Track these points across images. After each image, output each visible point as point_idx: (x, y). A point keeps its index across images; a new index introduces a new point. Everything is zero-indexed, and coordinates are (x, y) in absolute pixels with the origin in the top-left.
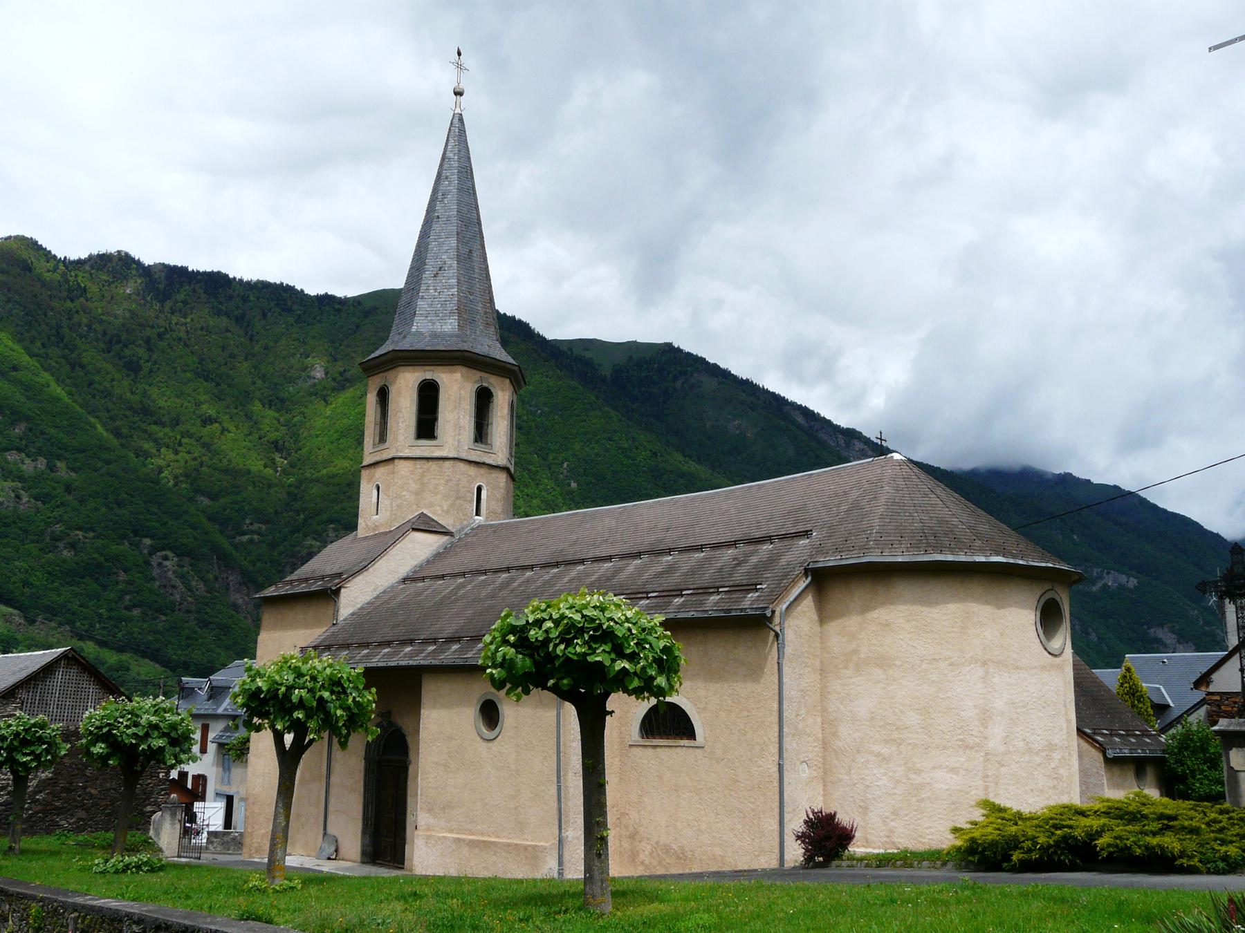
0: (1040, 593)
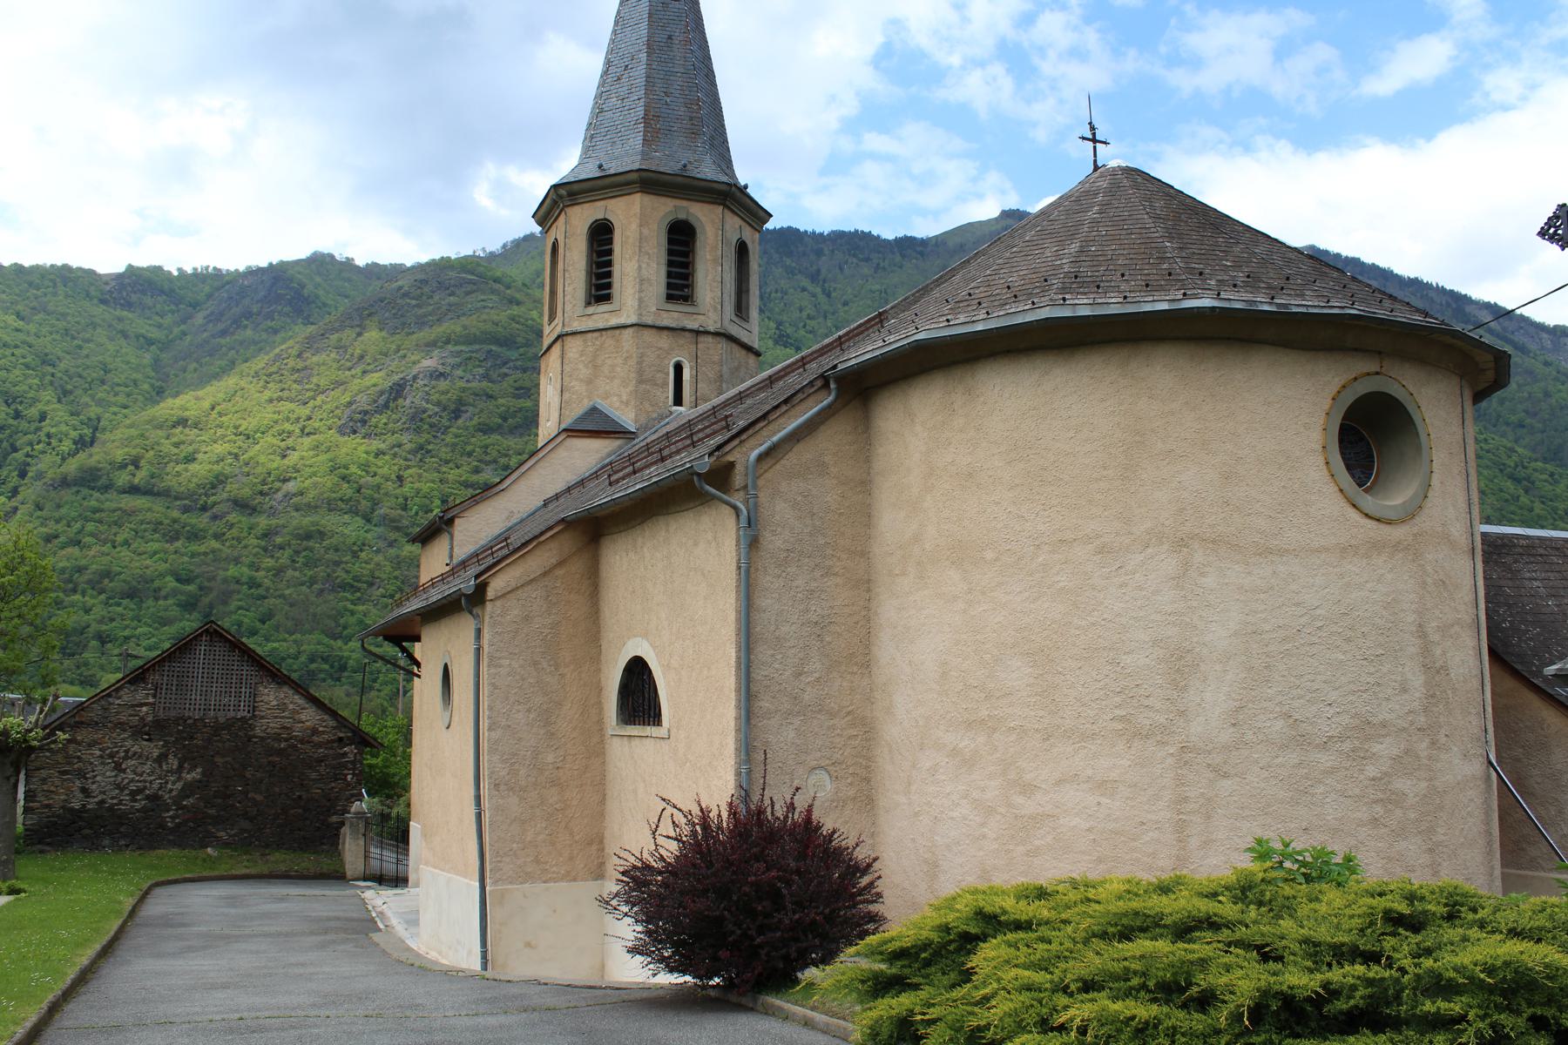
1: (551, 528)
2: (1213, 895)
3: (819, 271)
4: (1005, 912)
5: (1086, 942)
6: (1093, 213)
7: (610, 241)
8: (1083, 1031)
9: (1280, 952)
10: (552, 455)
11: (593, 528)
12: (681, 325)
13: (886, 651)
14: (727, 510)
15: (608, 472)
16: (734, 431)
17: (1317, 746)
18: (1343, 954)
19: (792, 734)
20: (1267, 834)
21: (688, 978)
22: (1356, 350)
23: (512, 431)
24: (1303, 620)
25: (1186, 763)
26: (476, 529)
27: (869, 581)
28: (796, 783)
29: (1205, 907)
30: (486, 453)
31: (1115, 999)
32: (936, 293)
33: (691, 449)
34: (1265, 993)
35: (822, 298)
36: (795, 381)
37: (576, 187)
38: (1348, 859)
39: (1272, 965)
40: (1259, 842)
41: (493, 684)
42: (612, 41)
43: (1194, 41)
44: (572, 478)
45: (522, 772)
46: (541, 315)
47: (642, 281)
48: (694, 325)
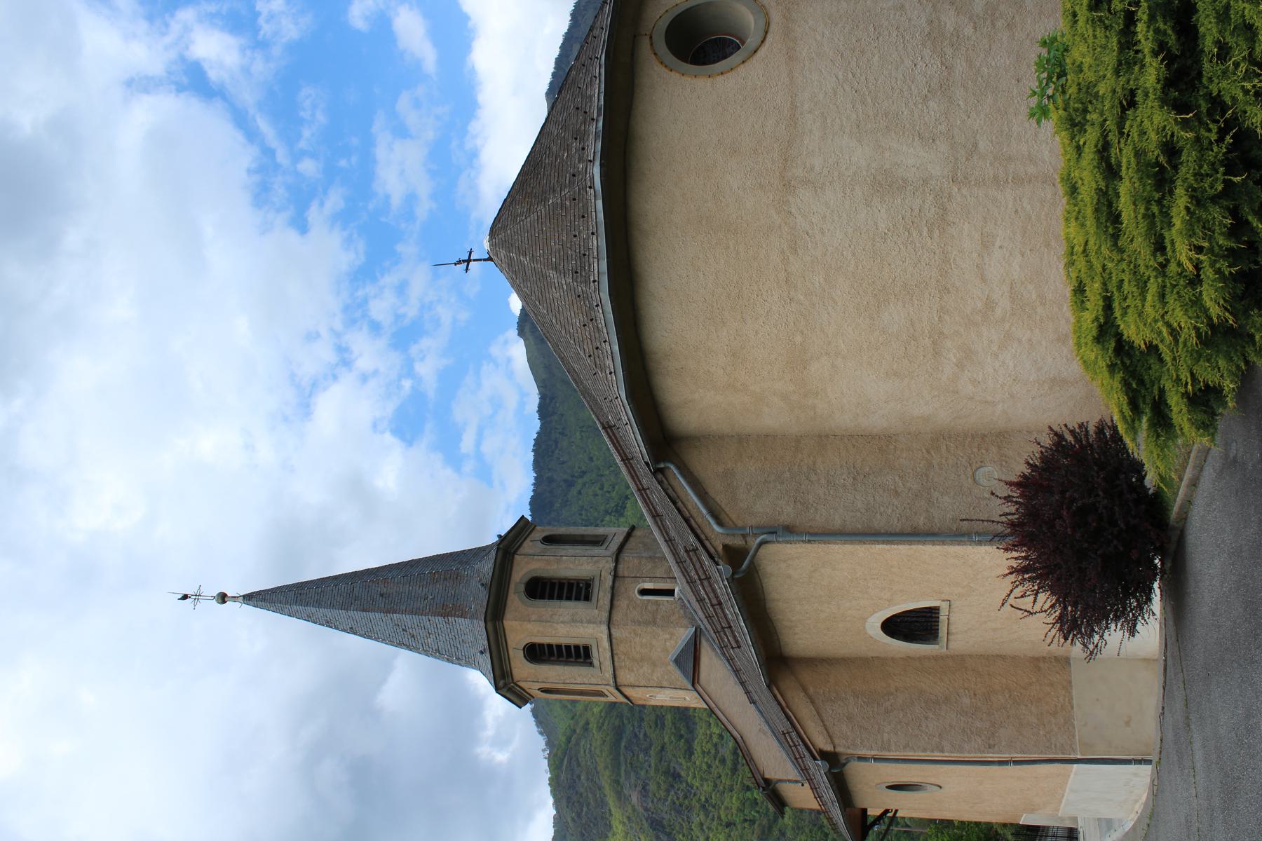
0: (658, 68)
1: (775, 696)
2: (1079, 149)
3: (565, 481)
4: (1097, 319)
5: (1121, 251)
6: (526, 261)
7: (541, 645)
8: (1199, 249)
9: (1127, 92)
10: (713, 696)
11: (776, 662)
12: (609, 589)
13: (876, 422)
14: (762, 551)
15: (727, 652)
16: (698, 545)
17: (949, 74)
18: (1128, 42)
19: (946, 498)
20: (1024, 111)
21: (1156, 585)
22: (632, 55)
23: (691, 731)
24: (847, 88)
25: (966, 178)
26: (773, 760)
27: (820, 436)
28: (987, 495)
29: (1089, 154)
30: (709, 752)
31: (1170, 225)
32: (588, 384)
33: (712, 581)
34: (1164, 101)
35: (586, 478)
36: (657, 495)
37: (498, 673)
38: (1044, 44)
39: (1139, 98)
40: (1032, 115)
41: (905, 748)
42: (383, 641)
43: (396, 201)
44: (732, 679)
45: (978, 724)
46: (596, 703)
47: (573, 621)
48: (610, 578)
